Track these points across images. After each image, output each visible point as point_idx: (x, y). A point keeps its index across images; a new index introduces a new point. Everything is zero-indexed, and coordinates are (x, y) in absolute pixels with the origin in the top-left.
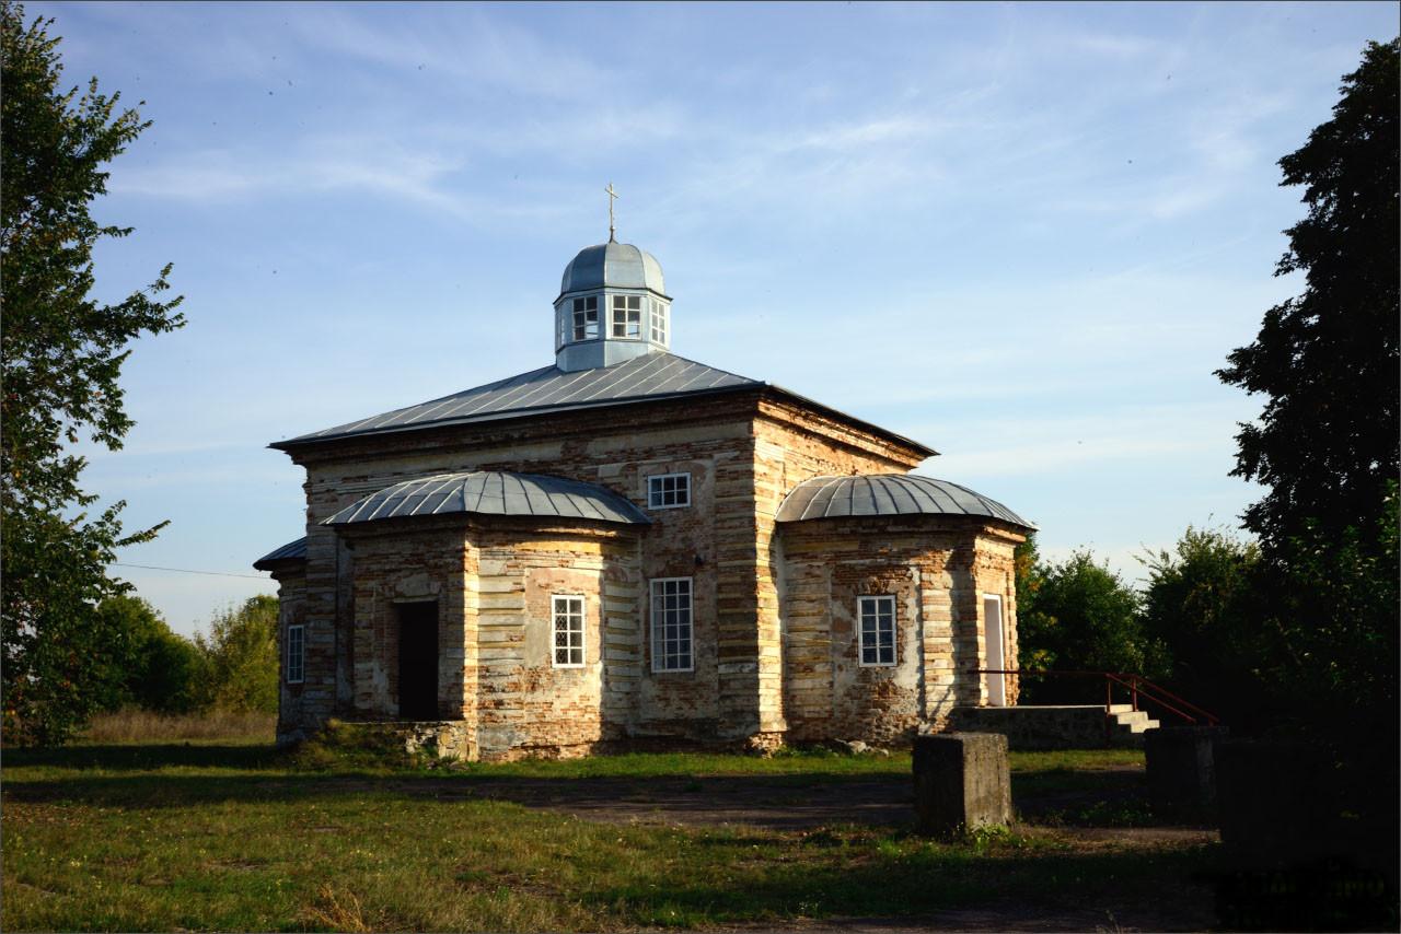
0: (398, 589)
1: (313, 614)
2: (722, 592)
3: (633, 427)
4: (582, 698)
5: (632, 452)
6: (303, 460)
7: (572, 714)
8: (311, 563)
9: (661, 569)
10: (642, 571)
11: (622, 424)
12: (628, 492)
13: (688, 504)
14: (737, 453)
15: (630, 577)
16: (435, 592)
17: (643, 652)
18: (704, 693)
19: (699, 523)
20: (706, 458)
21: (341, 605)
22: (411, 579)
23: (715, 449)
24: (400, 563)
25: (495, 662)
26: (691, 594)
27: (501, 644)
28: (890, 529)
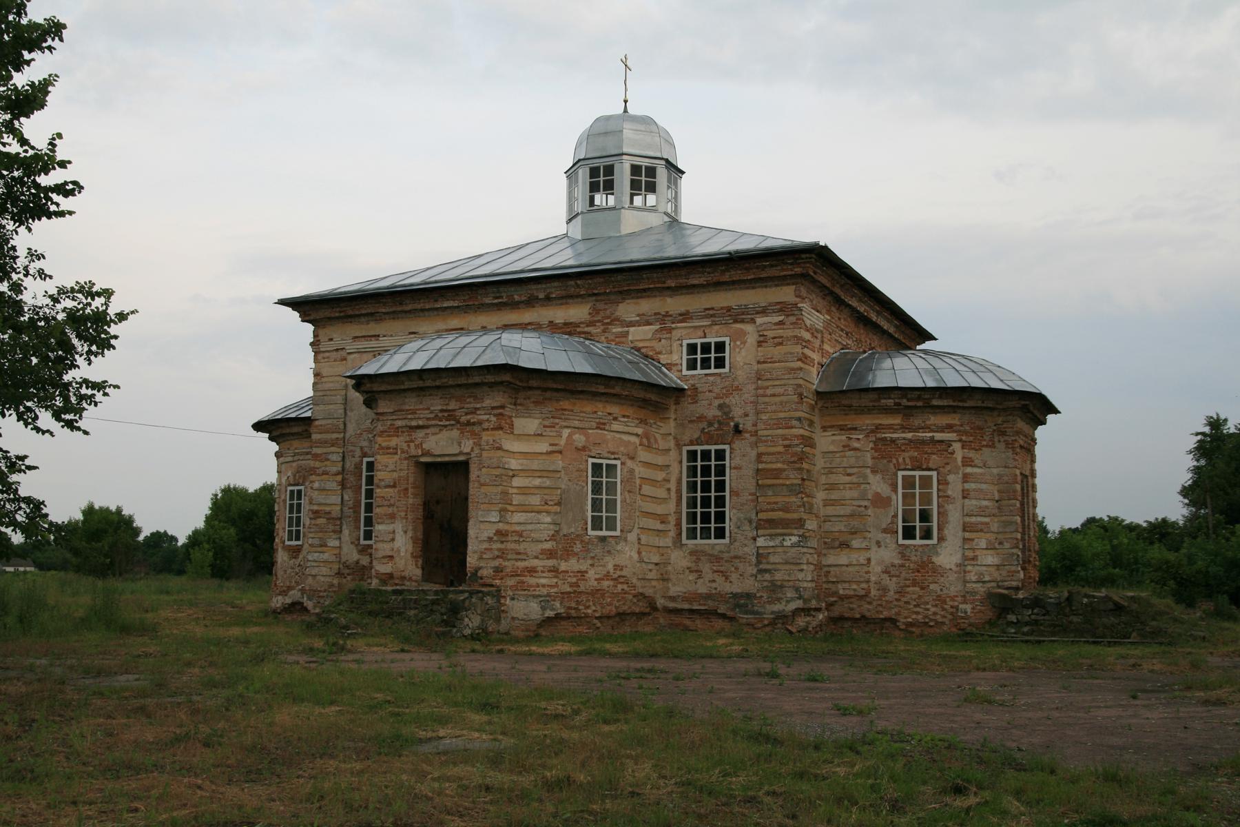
1: (319, 475)
2: (762, 462)
3: (669, 288)
4: (616, 567)
5: (667, 315)
6: (311, 318)
7: (606, 583)
8: (317, 423)
9: (696, 436)
10: (675, 438)
11: (657, 285)
12: (661, 357)
13: (727, 370)
14: (781, 318)
15: (662, 444)
16: (467, 450)
17: (673, 522)
18: (741, 566)
19: (738, 389)
21: (348, 465)
22: (439, 436)
23: (758, 313)
24: (428, 419)
25: (529, 527)
26: (727, 463)
27: (536, 508)
28: (935, 402)
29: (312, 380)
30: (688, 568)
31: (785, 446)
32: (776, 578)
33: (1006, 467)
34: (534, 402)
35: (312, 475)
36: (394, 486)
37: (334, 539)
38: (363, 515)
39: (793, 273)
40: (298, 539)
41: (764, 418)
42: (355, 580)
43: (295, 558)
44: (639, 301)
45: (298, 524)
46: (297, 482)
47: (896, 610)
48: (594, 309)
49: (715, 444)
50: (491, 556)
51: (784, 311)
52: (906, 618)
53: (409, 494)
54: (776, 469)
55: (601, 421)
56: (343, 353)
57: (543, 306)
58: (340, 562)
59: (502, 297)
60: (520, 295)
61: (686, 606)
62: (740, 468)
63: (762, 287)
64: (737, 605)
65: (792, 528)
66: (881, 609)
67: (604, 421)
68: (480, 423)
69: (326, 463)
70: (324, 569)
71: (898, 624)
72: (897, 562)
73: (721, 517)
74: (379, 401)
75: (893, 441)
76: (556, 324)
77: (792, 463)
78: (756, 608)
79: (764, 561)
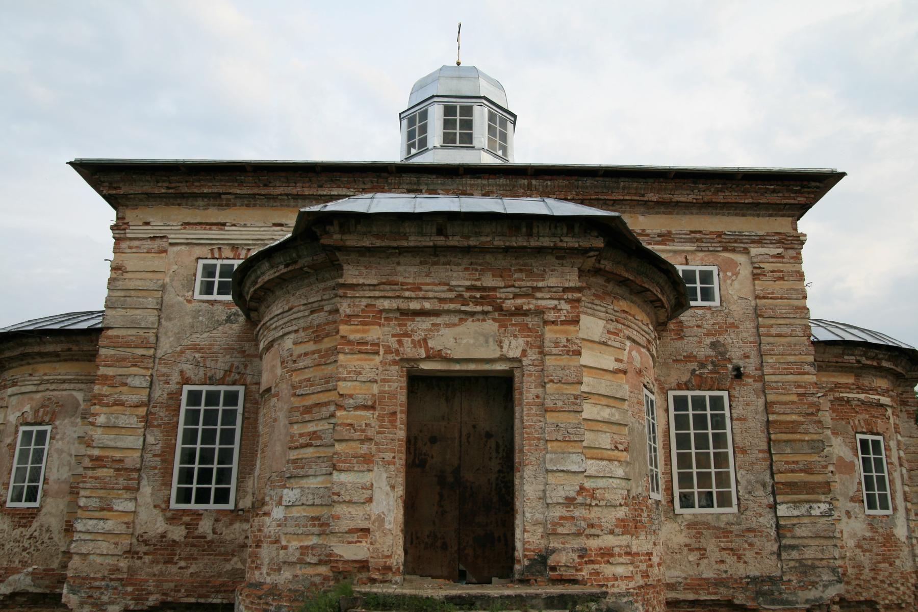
0: (431, 344)
1: (107, 405)
8: (110, 332)
9: (685, 378)
13: (716, 303)
14: (780, 251)
16: (515, 353)
18: (756, 541)
19: (733, 326)
20: (739, 252)
23: (753, 242)
24: (441, 300)
25: (601, 483)
26: (727, 412)
29: (107, 273)
30: (686, 546)
31: (799, 395)
32: (807, 556)
33: (910, 437)
35: (95, 404)
36: (373, 408)
37: (126, 499)
38: (177, 466)
39: (796, 202)
41: (770, 361)
42: (158, 563)
43: (25, 526)
46: (39, 420)
47: (874, 590)
49: (709, 390)
50: (574, 530)
51: (783, 243)
52: (884, 599)
53: (398, 423)
56: (163, 243)
58: (132, 534)
61: (691, 597)
62: (745, 420)
63: (754, 215)
64: (759, 593)
65: (818, 493)
66: (860, 590)
68: (540, 312)
69: (120, 389)
70: (105, 544)
71: (878, 607)
72: (868, 534)
73: (723, 480)
74: (345, 267)
75: (848, 401)
77: (808, 414)
78: (785, 596)
79: (789, 535)
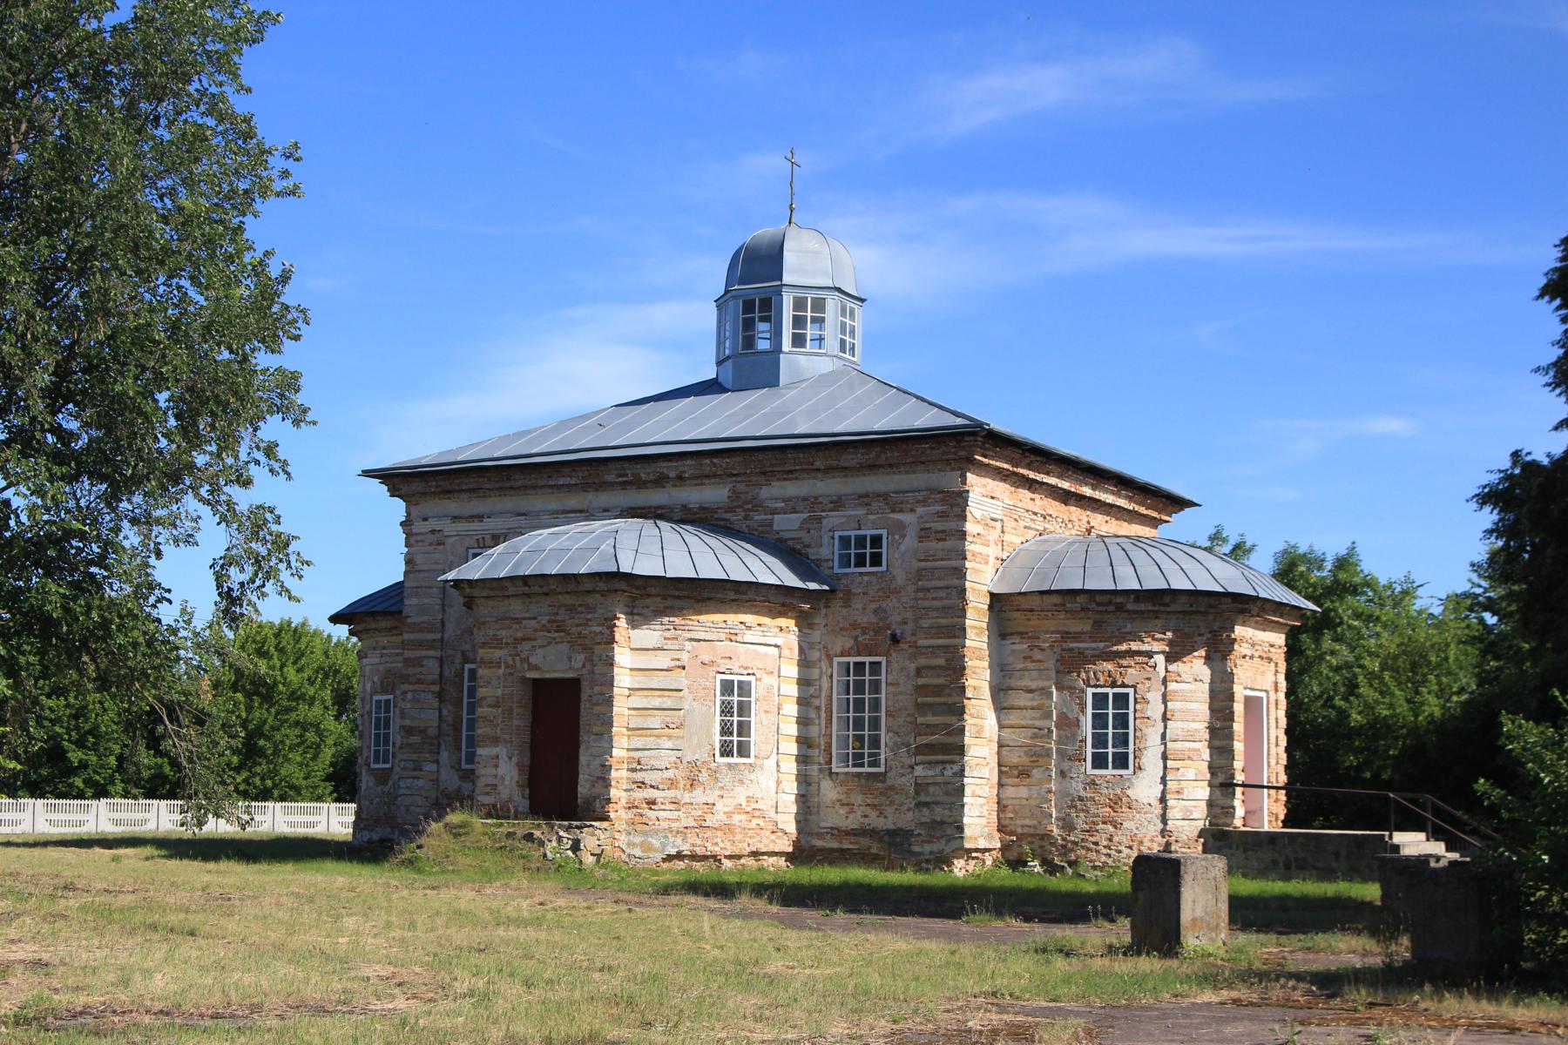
0: (531, 661)
7: (736, 818)
8: (409, 620)
12: (809, 550)
28: (1130, 607)
30: (838, 801)
34: (653, 611)
40: (386, 761)
44: (785, 483)
45: (387, 743)
48: (734, 492)
54: (937, 686)
55: (732, 631)
57: (674, 486)
59: (626, 476)
60: (648, 474)
67: (735, 631)
76: (690, 509)
